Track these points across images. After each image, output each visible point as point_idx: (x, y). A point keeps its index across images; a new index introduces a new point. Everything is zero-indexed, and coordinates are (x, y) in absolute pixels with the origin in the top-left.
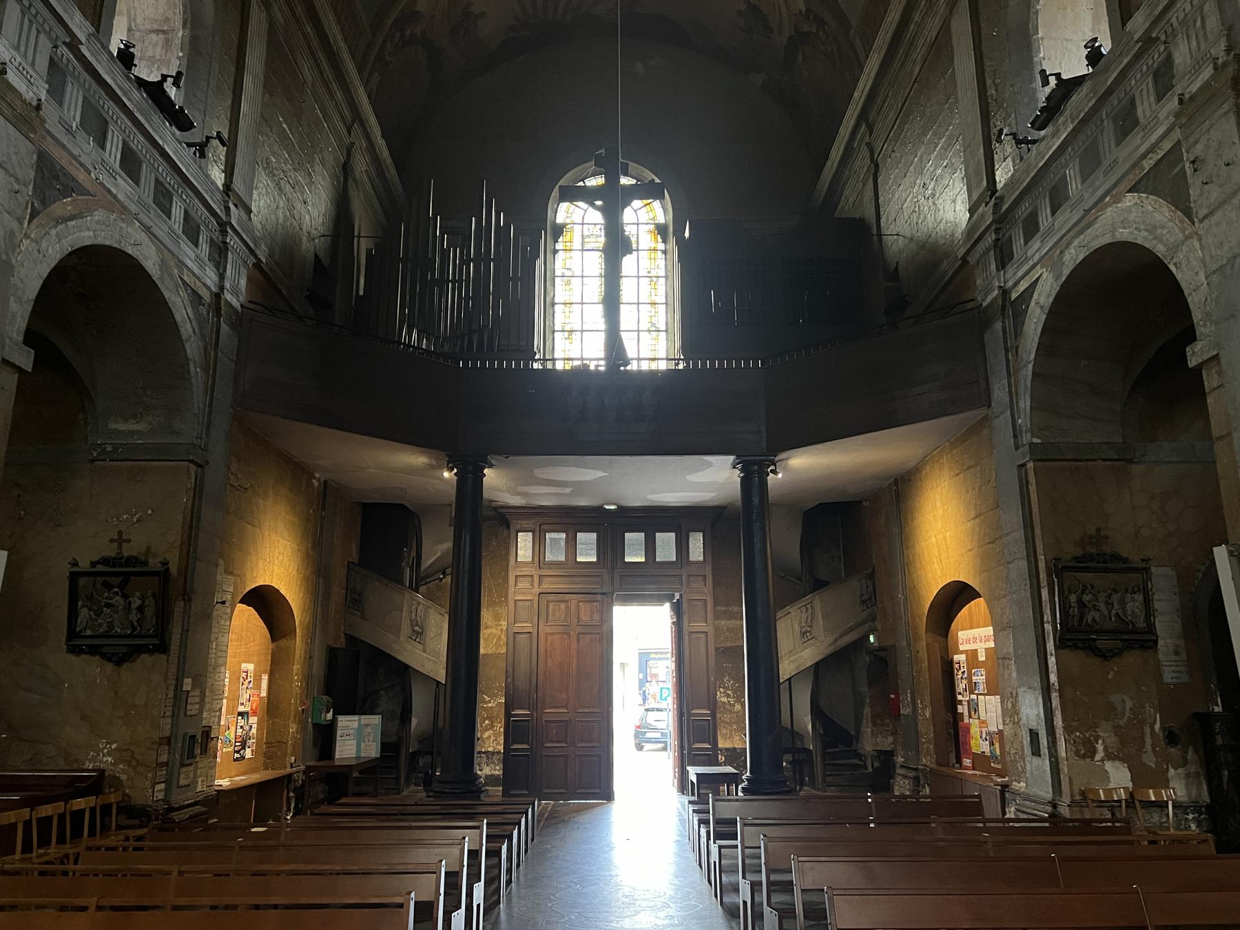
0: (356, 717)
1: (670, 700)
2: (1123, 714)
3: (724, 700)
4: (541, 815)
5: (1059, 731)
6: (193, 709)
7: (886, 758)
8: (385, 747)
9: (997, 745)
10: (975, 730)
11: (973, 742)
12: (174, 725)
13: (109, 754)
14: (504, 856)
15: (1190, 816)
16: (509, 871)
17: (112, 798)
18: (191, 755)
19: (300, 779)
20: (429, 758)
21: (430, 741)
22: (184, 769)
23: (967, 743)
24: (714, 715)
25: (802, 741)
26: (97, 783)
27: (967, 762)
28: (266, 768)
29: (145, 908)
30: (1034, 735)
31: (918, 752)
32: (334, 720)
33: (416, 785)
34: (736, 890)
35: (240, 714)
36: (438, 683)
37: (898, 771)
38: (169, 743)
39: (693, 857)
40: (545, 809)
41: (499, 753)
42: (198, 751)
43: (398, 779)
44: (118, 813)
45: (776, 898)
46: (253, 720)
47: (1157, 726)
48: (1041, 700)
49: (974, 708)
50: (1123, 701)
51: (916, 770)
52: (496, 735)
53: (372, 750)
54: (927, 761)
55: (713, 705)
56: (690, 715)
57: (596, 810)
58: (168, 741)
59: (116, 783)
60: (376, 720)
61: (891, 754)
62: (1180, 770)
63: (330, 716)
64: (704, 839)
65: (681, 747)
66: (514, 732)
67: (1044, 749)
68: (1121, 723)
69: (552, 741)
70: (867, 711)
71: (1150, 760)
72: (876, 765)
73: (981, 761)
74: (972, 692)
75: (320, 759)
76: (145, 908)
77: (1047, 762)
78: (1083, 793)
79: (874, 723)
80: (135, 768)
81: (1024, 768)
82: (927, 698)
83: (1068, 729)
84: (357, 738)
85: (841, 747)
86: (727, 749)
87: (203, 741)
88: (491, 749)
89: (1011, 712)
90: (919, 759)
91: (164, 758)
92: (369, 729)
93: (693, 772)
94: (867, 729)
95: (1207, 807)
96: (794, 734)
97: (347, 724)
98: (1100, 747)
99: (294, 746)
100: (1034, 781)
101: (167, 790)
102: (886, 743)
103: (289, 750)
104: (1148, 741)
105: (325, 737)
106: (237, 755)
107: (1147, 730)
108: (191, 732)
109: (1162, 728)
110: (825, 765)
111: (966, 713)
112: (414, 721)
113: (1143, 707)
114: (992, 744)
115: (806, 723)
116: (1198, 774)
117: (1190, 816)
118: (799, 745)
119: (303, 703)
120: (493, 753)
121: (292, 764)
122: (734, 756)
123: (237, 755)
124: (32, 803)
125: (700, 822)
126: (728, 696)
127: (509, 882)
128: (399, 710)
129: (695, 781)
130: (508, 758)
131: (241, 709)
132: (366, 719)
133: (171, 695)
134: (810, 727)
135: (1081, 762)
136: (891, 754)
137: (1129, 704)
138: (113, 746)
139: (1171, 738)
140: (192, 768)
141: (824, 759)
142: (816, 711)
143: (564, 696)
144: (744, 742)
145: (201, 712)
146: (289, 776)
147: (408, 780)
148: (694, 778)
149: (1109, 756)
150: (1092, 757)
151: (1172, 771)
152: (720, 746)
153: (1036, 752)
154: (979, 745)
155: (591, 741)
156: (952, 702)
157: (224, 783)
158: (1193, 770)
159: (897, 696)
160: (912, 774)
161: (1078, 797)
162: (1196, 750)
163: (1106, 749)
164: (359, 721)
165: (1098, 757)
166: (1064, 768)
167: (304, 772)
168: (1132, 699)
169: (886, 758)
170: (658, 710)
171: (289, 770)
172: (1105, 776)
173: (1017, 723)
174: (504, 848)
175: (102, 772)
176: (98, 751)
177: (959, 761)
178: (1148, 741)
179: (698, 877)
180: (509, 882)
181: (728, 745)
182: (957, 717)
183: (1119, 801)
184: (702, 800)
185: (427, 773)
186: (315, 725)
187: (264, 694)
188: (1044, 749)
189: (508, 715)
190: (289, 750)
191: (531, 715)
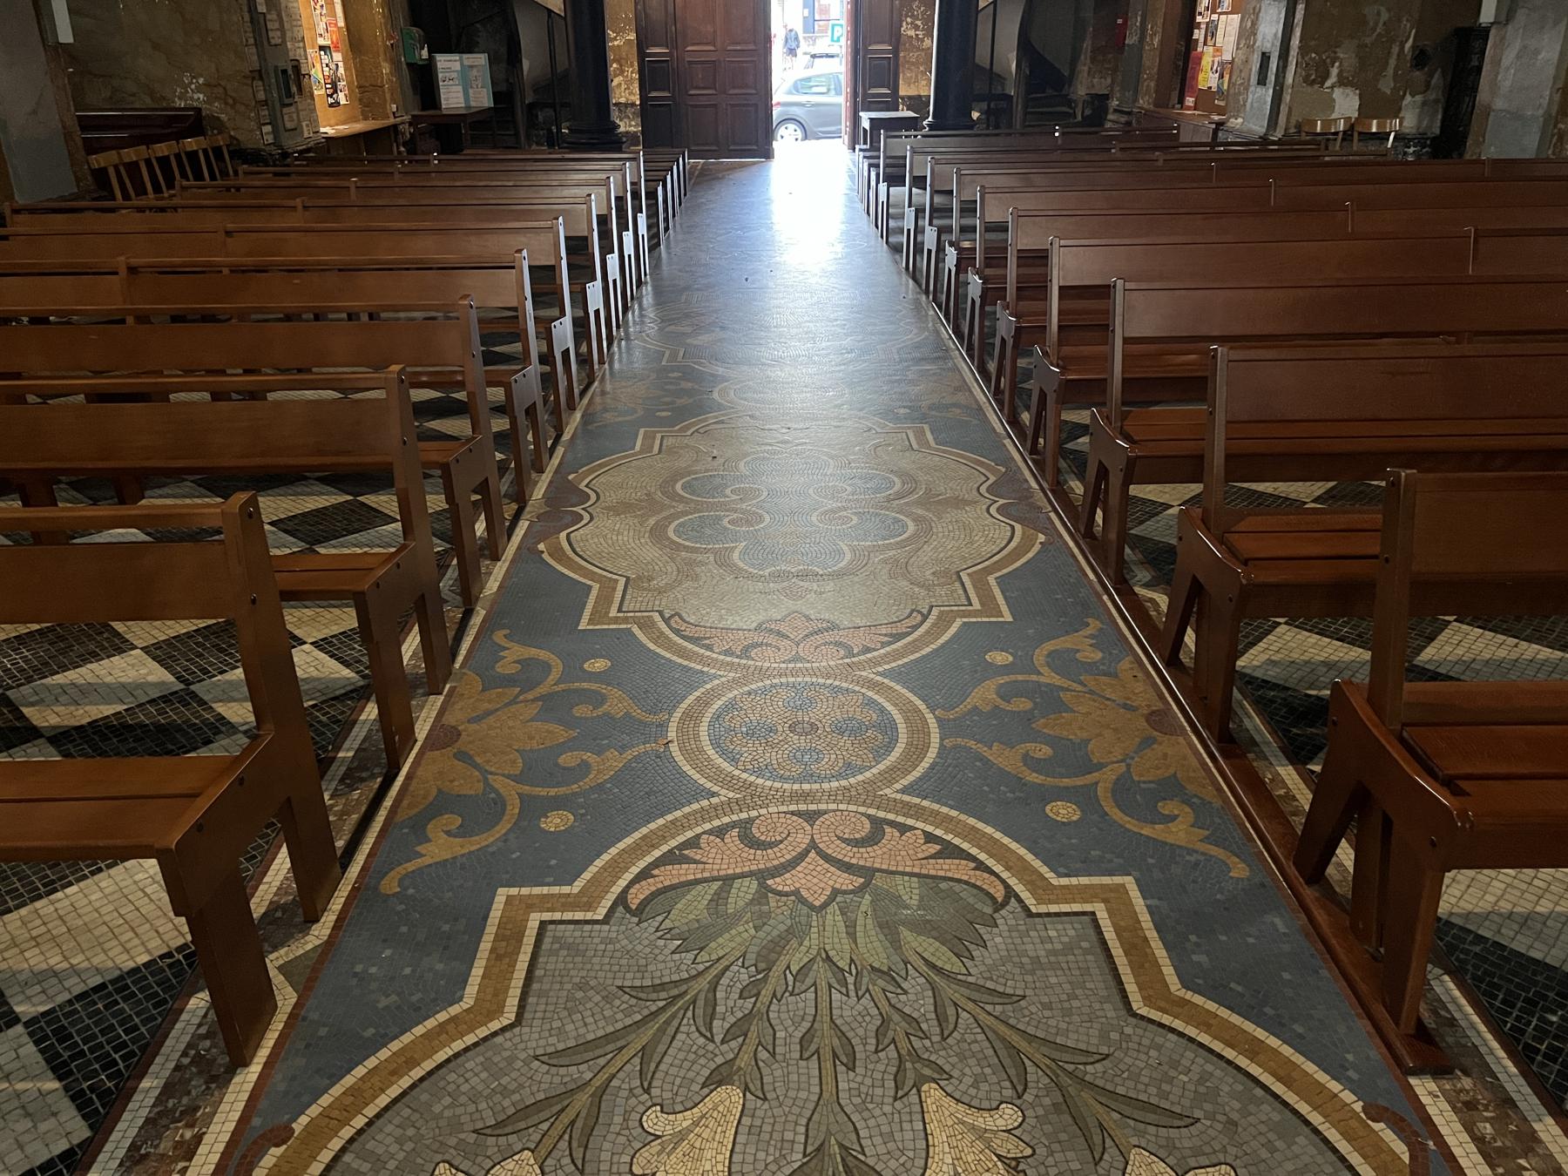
0: (456, 57)
1: (843, 41)
2: (1374, 29)
3: (912, 33)
4: (691, 173)
5: (1294, 52)
6: (275, 37)
7: (1099, 102)
8: (497, 96)
9: (1227, 77)
10: (1206, 62)
11: (1201, 76)
12: (262, 56)
13: (198, 90)
14: (660, 199)
15: (1412, 150)
16: (666, 220)
17: (221, 141)
18: (290, 95)
19: (407, 130)
20: (550, 112)
21: (553, 89)
22: (285, 110)
23: (1195, 78)
24: (896, 52)
25: (1003, 85)
26: (195, 123)
27: (1190, 101)
28: (366, 119)
29: (208, 318)
30: (1265, 58)
31: (1136, 91)
32: (431, 59)
33: (538, 144)
34: (902, 216)
35: (322, 48)
36: (549, 11)
37: (1110, 117)
38: (261, 78)
39: (862, 207)
40: (694, 167)
41: (633, 104)
42: (294, 89)
43: (517, 135)
44: (231, 158)
45: (937, 199)
46: (338, 57)
47: (1408, 45)
48: (1283, 15)
49: (1212, 30)
50: (1379, 14)
51: (1129, 113)
52: (629, 82)
53: (483, 99)
54: (1145, 102)
55: (896, 39)
56: (867, 52)
57: (754, 168)
58: (259, 75)
59: (220, 126)
60: (481, 59)
61: (1105, 98)
62: (1419, 98)
63: (425, 53)
64: (873, 183)
65: (855, 94)
66: (650, 75)
67: (1271, 77)
68: (1368, 41)
69: (697, 88)
70: (1087, 45)
71: (1386, 86)
72: (1088, 112)
73: (1206, 99)
74: (1213, 12)
75: (423, 109)
76: (208, 318)
77: (1271, 91)
78: (1299, 126)
79: (1093, 60)
80: (232, 107)
81: (1245, 101)
82: (1160, 21)
83: (1304, 49)
84: (463, 82)
85: (1050, 92)
86: (910, 98)
87: (292, 79)
88: (623, 100)
89: (1247, 34)
90: (1135, 100)
91: (261, 96)
92: (475, 72)
93: (865, 118)
94: (1083, 69)
95: (1433, 140)
96: (993, 76)
97: (448, 64)
98: (1334, 71)
99: (392, 91)
100: (1251, 118)
101: (275, 132)
102: (1101, 85)
103: (388, 96)
104: (1392, 62)
105: (424, 82)
106: (331, 100)
107: (1395, 50)
108: (282, 65)
109: (1413, 47)
110: (1026, 114)
111: (1202, 40)
112: (526, 64)
113: (1400, 21)
114: (1221, 76)
115: (1010, 61)
116: (1436, 101)
117: (1412, 150)
118: (999, 90)
119: (390, 37)
120: (626, 105)
121: (395, 112)
122: (917, 103)
123: (331, 100)
124: (149, 140)
125: (870, 166)
126: (917, 28)
127: (666, 229)
128: (503, 50)
129: (868, 127)
130: (646, 111)
131: (321, 42)
132: (470, 59)
133: (247, 18)
134: (1014, 66)
135: (1309, 89)
136: (1105, 98)
137: (1385, 16)
138: (201, 81)
139: (1420, 58)
140: (292, 109)
141: (1026, 107)
142: (1025, 45)
143: (710, 28)
144: (927, 88)
145: (284, 42)
146: (395, 126)
147: (528, 137)
148: (866, 124)
149: (1343, 82)
150: (1322, 84)
151: (1408, 98)
152: (902, 93)
153: (1262, 81)
154: (1208, 79)
155: (747, 87)
156: (1191, 25)
157: (329, 131)
158: (1433, 97)
159: (1125, 22)
160: (1124, 119)
161: (1292, 130)
162: (1444, 74)
163: (1340, 75)
164: (461, 60)
165: (1328, 83)
166: (1287, 98)
167: (410, 124)
168: (1389, 10)
169: (1099, 102)
170: (828, 56)
171: (392, 121)
172: (1330, 104)
173: (1251, 47)
174: (660, 189)
175: (198, 110)
176: (186, 87)
177: (1181, 101)
178: (1392, 62)
179: (865, 224)
180: (666, 229)
181: (912, 92)
182: (1190, 44)
183: (1336, 133)
184: (875, 147)
185: (550, 130)
186: (409, 65)
187: (341, 23)
188: (1271, 77)
189: (642, 55)
190: (388, 96)
191: (670, 54)
